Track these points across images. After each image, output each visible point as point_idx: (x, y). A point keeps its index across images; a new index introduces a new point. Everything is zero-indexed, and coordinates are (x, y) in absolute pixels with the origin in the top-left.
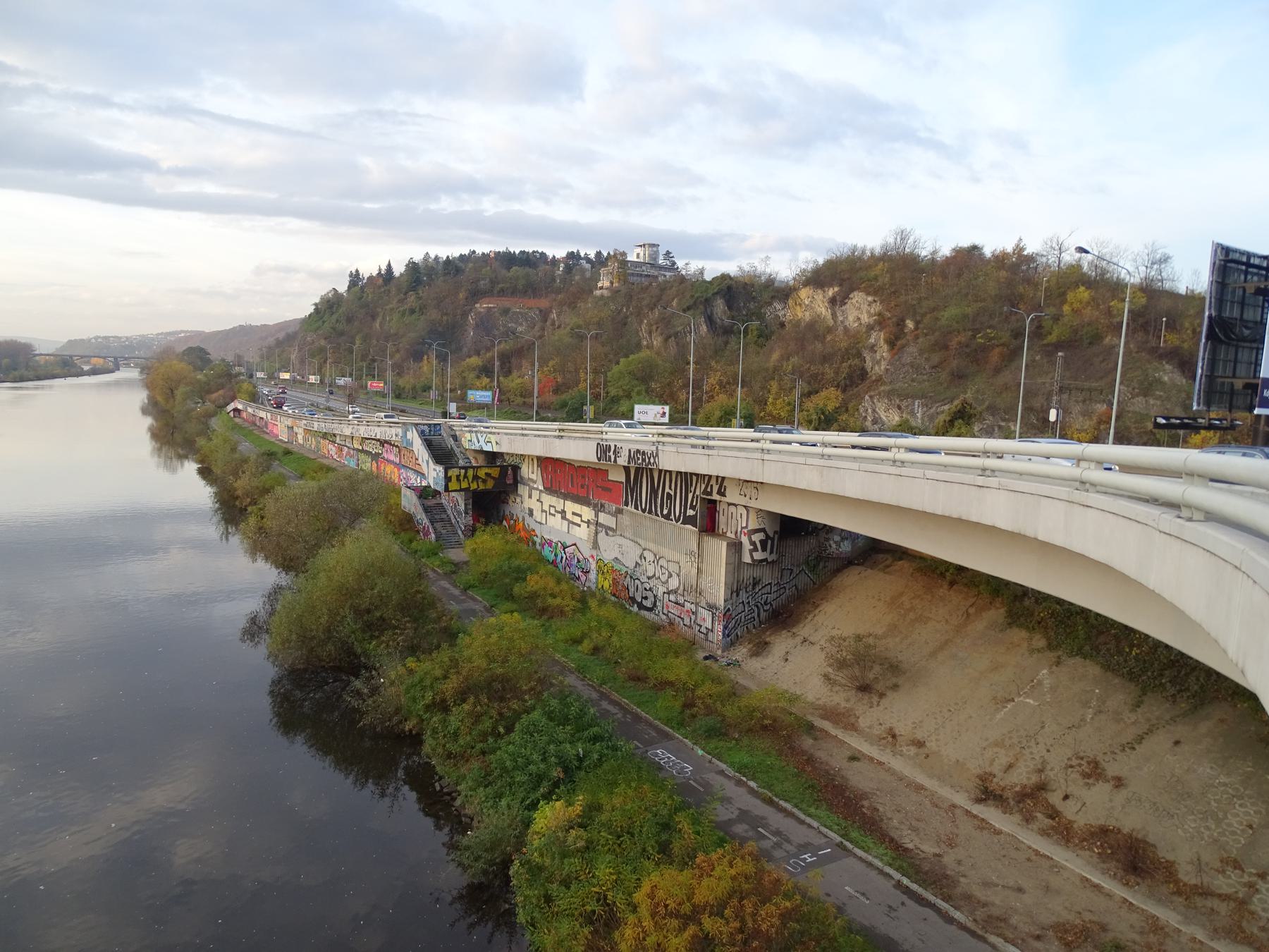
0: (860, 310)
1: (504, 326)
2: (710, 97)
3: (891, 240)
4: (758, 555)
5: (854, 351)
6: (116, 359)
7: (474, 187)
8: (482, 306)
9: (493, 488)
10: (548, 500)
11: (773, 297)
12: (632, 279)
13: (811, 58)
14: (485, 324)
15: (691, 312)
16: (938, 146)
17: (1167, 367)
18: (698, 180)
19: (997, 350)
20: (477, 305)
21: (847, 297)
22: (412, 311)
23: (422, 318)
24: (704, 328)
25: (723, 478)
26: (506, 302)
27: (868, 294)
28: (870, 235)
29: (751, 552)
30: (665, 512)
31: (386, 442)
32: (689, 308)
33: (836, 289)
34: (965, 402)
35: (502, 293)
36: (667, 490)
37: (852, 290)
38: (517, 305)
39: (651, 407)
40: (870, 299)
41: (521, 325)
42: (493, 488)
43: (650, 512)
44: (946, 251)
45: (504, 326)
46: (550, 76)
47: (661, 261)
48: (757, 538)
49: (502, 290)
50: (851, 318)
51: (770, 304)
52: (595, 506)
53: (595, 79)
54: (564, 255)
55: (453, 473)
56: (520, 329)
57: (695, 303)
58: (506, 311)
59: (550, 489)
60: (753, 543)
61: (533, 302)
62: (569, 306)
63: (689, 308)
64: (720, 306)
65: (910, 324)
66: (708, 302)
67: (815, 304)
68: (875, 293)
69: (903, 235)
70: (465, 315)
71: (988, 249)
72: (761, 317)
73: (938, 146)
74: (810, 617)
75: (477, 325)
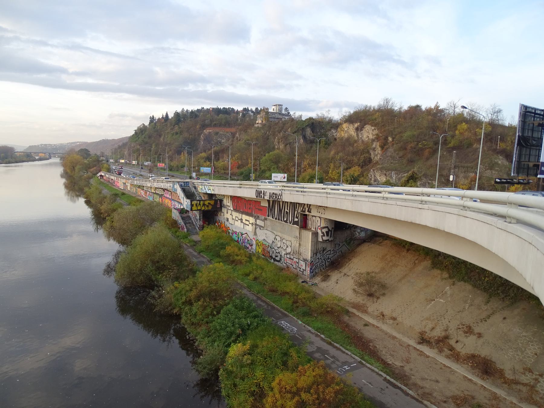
0: (369, 133)
1: (216, 140)
2: (304, 41)
3: (382, 103)
4: (325, 238)
5: (366, 151)
6: (50, 154)
7: (203, 80)
8: (207, 131)
9: (211, 209)
10: (235, 214)
11: (331, 127)
12: (271, 120)
13: (348, 25)
14: (208, 139)
15: (296, 134)
16: (402, 63)
17: (500, 157)
18: (299, 77)
19: (427, 150)
20: (205, 131)
21: (363, 127)
22: (177, 133)
23: (181, 136)
24: (302, 141)
25: (310, 205)
26: (217, 130)
27: (372, 126)
28: (373, 101)
29: (322, 236)
30: (285, 219)
31: (165, 189)
32: (295, 132)
33: (358, 124)
34: (414, 172)
35: (215, 125)
36: (286, 210)
37: (365, 124)
38: (222, 131)
39: (279, 174)
40: (373, 128)
41: (223, 139)
42: (211, 209)
43: (279, 219)
44: (405, 108)
45: (216, 140)
46: (236, 33)
47: (283, 112)
48: (324, 230)
49: (215, 124)
50: (365, 136)
51: (330, 130)
52: (255, 217)
53: (255, 34)
54: (242, 109)
55: (194, 203)
56: (223, 141)
57: (298, 130)
58: (217, 133)
59: (236, 210)
60: (323, 233)
61: (228, 130)
62: (244, 131)
63: (295, 132)
64: (308, 131)
65: (390, 139)
66: (303, 129)
67: (349, 130)
68: (375, 126)
69: (387, 101)
70: (199, 135)
71: (424, 107)
72: (326, 136)
73: (402, 63)
74: (347, 265)
75: (204, 139)
